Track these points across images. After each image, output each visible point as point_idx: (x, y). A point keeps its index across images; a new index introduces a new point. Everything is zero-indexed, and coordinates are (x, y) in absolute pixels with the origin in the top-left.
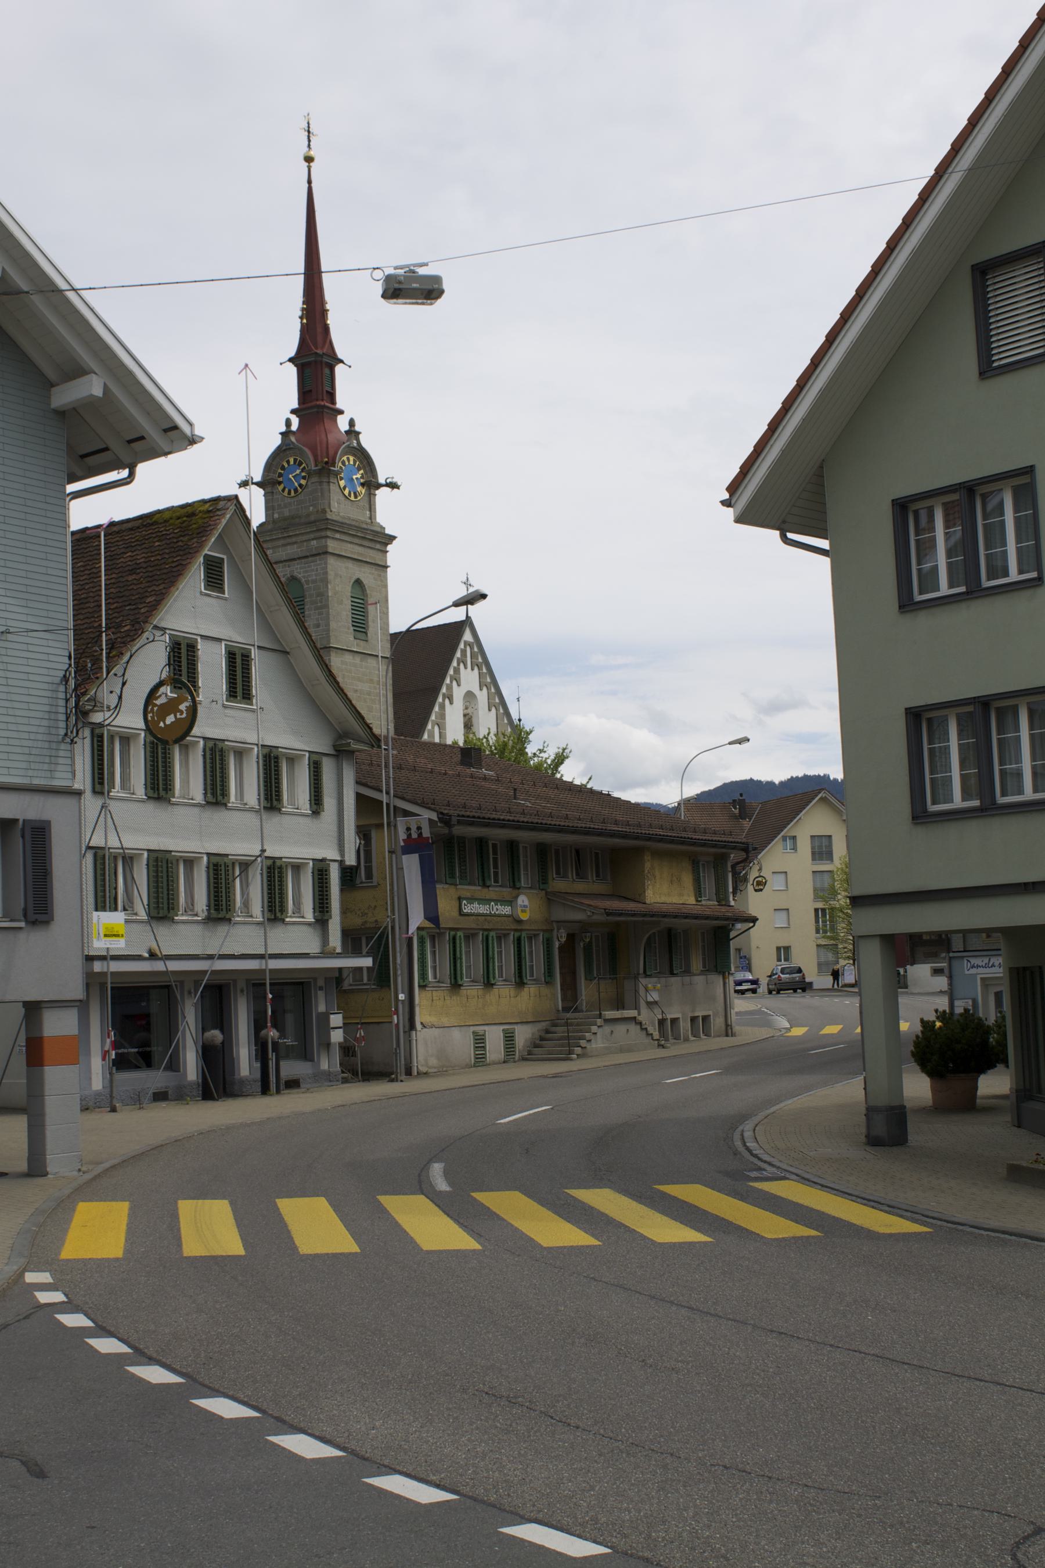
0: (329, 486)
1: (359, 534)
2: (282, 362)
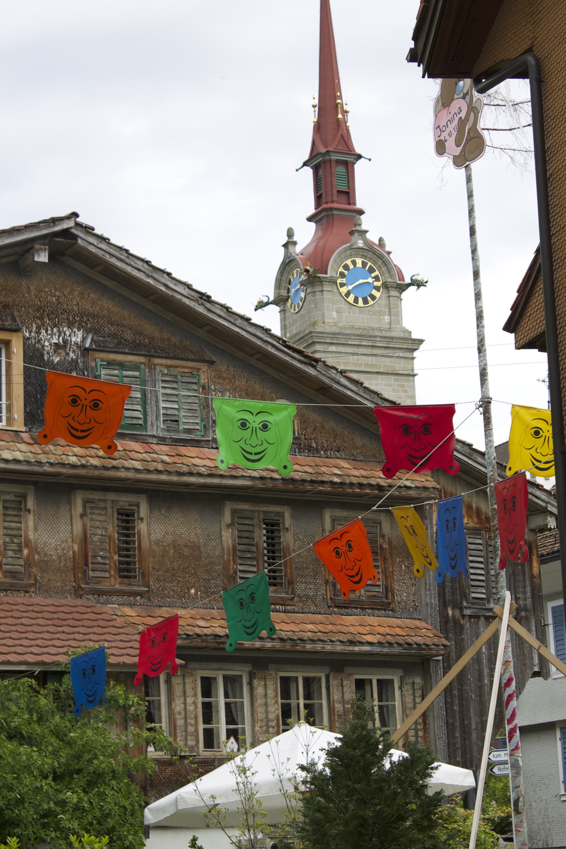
0: (323, 295)
1: (364, 344)
2: (298, 168)
